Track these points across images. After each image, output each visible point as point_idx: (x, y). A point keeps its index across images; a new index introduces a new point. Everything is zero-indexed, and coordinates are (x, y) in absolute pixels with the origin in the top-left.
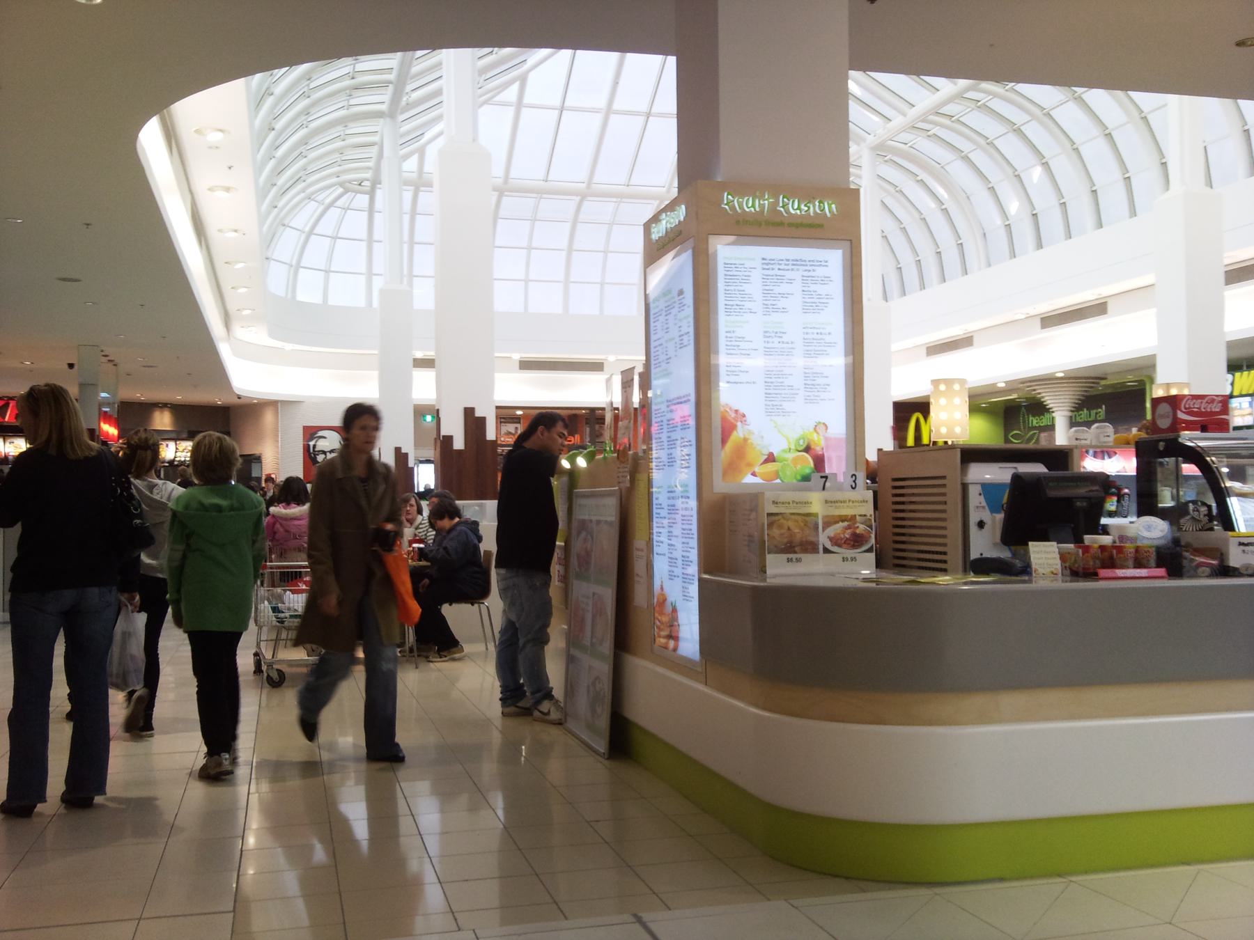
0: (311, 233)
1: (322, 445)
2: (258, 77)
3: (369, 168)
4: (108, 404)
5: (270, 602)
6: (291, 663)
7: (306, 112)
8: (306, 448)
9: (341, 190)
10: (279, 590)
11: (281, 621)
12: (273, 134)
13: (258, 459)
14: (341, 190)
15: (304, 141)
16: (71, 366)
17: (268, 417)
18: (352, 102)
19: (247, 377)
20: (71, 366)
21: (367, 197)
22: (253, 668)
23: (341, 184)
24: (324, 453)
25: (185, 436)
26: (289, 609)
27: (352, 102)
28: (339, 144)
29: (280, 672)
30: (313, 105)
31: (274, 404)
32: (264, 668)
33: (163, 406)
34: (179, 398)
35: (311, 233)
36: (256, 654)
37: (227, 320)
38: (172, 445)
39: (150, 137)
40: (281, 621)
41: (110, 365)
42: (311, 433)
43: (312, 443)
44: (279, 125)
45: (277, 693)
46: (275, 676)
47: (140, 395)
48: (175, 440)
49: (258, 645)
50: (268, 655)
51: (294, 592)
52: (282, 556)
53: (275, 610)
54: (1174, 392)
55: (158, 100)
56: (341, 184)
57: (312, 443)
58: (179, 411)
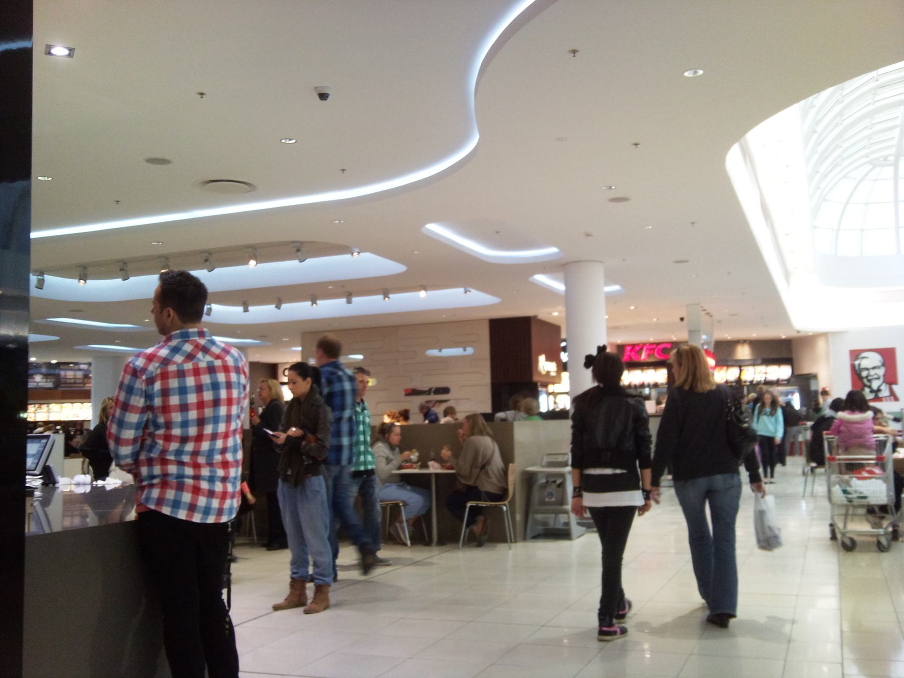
0: (847, 203)
1: (865, 363)
2: (802, 102)
3: (892, 146)
4: (707, 343)
5: (840, 486)
6: (861, 534)
7: (841, 113)
8: (853, 367)
9: (871, 167)
10: (846, 477)
11: (850, 501)
12: (816, 135)
13: (815, 377)
14: (871, 167)
15: (840, 135)
16: (682, 319)
17: (821, 345)
18: (877, 98)
19: (801, 320)
20: (682, 319)
21: (892, 169)
22: (828, 535)
23: (870, 162)
24: (867, 369)
25: (760, 362)
26: (856, 492)
27: (877, 98)
28: (867, 132)
29: (852, 540)
30: (882, 87)
31: (825, 335)
32: (839, 536)
33: (744, 342)
34: (755, 335)
35: (847, 203)
36: (831, 525)
37: (787, 275)
38: (751, 368)
39: (733, 159)
40: (850, 501)
41: (707, 317)
42: (855, 354)
43: (857, 363)
44: (819, 129)
45: (850, 557)
46: (848, 542)
47: (728, 336)
48: (754, 365)
49: (832, 518)
50: (840, 525)
51: (859, 478)
52: (847, 450)
53: (845, 492)
54: (370, 467)
55: (737, 132)
56: (870, 162)
57: (857, 363)
58: (755, 344)
